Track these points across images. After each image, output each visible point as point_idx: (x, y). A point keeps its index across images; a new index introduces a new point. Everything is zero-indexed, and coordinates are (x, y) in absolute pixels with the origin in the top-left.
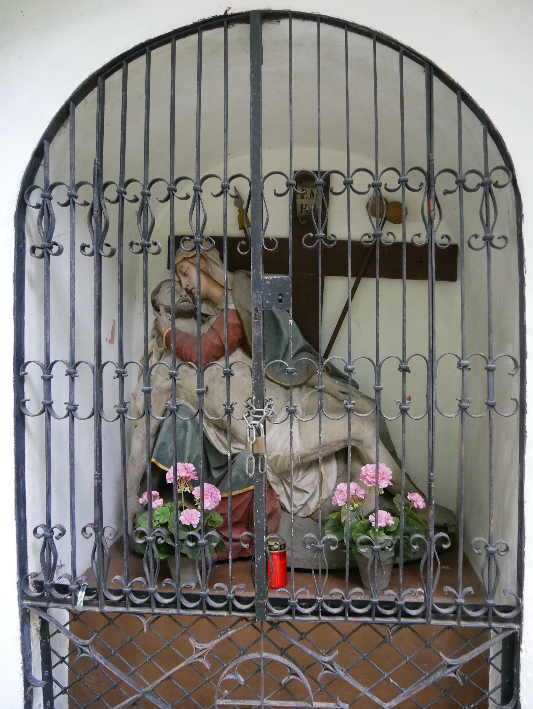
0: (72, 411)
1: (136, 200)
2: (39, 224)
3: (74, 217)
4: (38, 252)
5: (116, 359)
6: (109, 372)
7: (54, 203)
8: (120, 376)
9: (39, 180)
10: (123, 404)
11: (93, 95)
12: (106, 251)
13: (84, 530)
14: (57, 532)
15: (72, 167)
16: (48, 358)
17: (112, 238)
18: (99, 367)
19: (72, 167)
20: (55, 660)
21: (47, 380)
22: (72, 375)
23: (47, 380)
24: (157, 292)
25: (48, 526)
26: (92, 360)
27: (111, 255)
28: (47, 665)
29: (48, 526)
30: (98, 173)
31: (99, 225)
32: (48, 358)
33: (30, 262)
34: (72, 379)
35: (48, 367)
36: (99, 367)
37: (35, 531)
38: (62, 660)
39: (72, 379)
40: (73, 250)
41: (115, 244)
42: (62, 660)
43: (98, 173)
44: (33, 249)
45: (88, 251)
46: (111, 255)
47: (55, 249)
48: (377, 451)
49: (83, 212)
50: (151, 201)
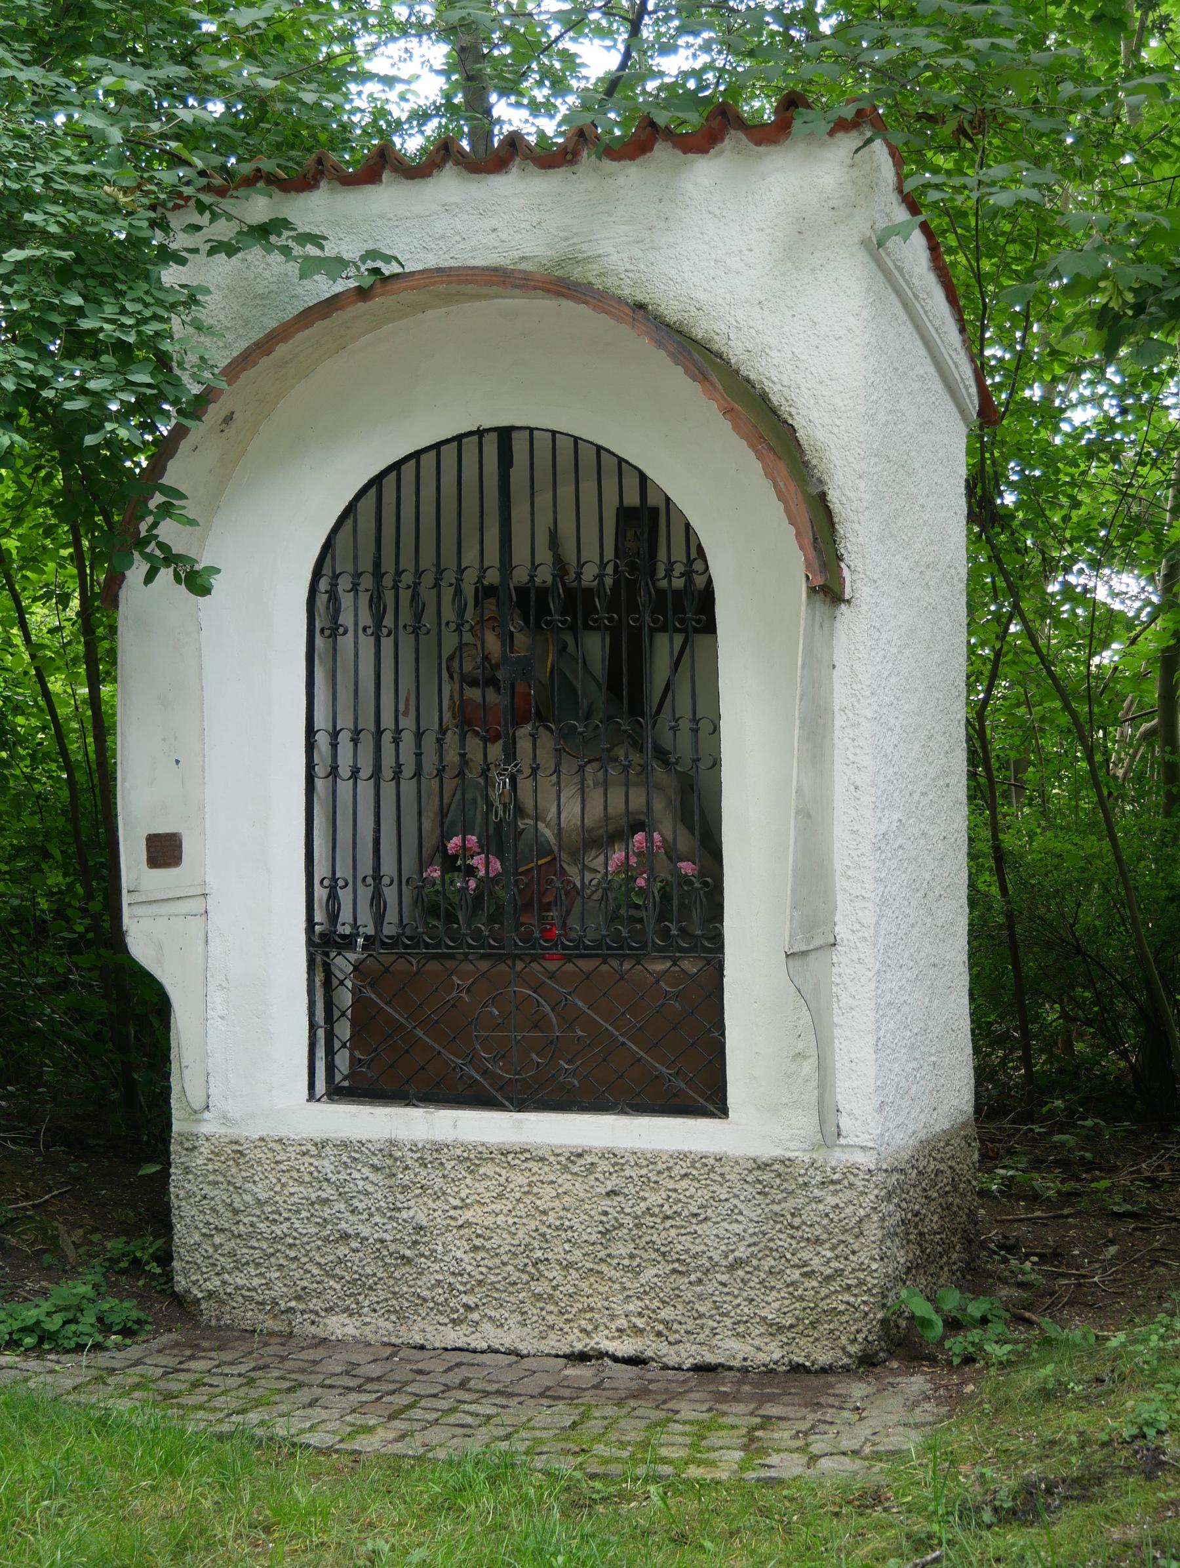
0: (355, 773)
1: (409, 587)
2: (328, 608)
3: (320, 893)
4: (327, 632)
5: (392, 727)
6: (387, 738)
7: (340, 588)
8: (396, 741)
9: (327, 570)
10: (399, 765)
11: (373, 490)
12: (385, 631)
13: (364, 879)
14: (341, 883)
15: (355, 558)
16: (334, 726)
17: (388, 621)
18: (379, 733)
19: (355, 558)
20: (337, 1045)
21: (334, 746)
22: (355, 741)
23: (334, 746)
24: (451, 658)
25: (334, 879)
26: (372, 728)
27: (389, 635)
28: (330, 1053)
29: (334, 879)
30: (377, 564)
31: (378, 609)
32: (334, 726)
33: (319, 641)
34: (356, 745)
35: (335, 734)
36: (379, 733)
37: (322, 882)
38: (344, 1046)
39: (356, 745)
40: (356, 631)
41: (391, 625)
42: (344, 1046)
43: (377, 564)
44: (322, 631)
45: (369, 631)
46: (389, 635)
47: (341, 630)
48: (675, 832)
49: (364, 598)
50: (422, 590)
